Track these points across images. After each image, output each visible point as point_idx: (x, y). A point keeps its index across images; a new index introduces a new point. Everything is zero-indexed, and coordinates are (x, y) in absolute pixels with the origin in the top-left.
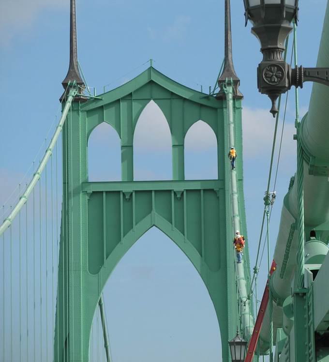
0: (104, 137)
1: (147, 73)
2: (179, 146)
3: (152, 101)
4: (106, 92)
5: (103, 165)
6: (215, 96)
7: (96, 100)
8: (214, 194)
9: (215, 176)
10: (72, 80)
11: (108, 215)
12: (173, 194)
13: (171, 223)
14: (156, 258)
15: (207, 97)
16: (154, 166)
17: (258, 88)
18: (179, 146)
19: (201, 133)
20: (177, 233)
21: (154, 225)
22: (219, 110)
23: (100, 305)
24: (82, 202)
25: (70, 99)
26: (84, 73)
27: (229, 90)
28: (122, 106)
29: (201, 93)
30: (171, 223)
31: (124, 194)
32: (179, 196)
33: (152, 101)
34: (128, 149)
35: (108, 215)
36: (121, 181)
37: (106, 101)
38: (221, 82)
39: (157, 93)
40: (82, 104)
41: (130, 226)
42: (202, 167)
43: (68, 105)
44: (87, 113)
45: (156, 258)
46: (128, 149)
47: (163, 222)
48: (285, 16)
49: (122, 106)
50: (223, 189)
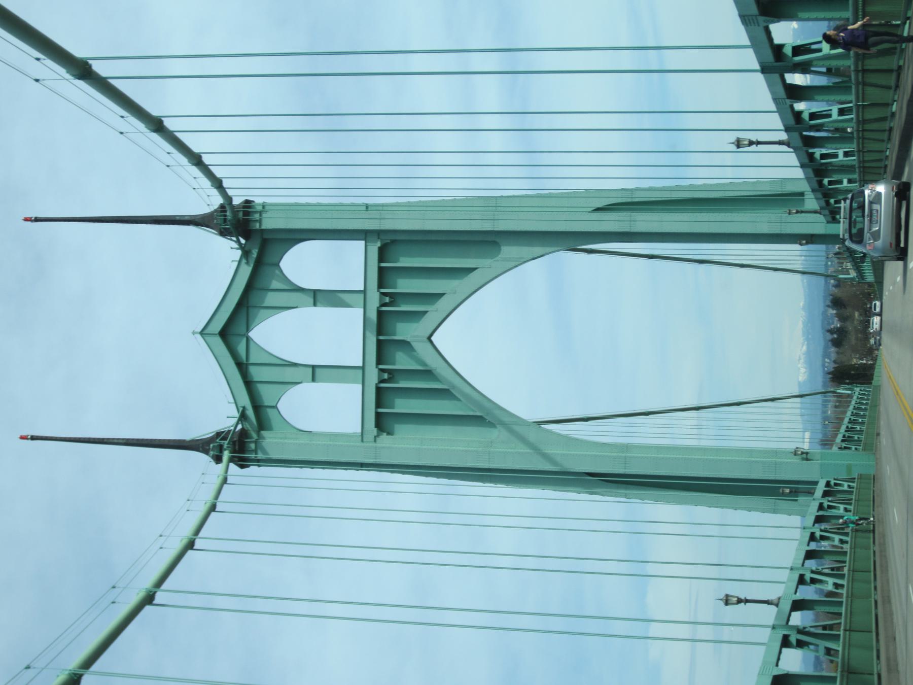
1: (208, 338)
2: (318, 297)
3: (251, 334)
4: (232, 401)
5: (330, 410)
6: (243, 241)
7: (243, 417)
8: (390, 246)
9: (359, 246)
12: (384, 309)
13: (426, 312)
14: (487, 337)
15: (246, 254)
16: (340, 336)
19: (302, 264)
20: (443, 305)
21: (429, 338)
22: (266, 236)
23: (540, 423)
24: (406, 442)
26: (204, 430)
29: (240, 262)
30: (426, 312)
31: (382, 381)
32: (387, 299)
33: (251, 334)
34: (315, 372)
36: (360, 386)
37: (245, 401)
39: (240, 327)
41: (428, 373)
44: (262, 429)
45: (487, 337)
46: (315, 372)
48: (805, 133)
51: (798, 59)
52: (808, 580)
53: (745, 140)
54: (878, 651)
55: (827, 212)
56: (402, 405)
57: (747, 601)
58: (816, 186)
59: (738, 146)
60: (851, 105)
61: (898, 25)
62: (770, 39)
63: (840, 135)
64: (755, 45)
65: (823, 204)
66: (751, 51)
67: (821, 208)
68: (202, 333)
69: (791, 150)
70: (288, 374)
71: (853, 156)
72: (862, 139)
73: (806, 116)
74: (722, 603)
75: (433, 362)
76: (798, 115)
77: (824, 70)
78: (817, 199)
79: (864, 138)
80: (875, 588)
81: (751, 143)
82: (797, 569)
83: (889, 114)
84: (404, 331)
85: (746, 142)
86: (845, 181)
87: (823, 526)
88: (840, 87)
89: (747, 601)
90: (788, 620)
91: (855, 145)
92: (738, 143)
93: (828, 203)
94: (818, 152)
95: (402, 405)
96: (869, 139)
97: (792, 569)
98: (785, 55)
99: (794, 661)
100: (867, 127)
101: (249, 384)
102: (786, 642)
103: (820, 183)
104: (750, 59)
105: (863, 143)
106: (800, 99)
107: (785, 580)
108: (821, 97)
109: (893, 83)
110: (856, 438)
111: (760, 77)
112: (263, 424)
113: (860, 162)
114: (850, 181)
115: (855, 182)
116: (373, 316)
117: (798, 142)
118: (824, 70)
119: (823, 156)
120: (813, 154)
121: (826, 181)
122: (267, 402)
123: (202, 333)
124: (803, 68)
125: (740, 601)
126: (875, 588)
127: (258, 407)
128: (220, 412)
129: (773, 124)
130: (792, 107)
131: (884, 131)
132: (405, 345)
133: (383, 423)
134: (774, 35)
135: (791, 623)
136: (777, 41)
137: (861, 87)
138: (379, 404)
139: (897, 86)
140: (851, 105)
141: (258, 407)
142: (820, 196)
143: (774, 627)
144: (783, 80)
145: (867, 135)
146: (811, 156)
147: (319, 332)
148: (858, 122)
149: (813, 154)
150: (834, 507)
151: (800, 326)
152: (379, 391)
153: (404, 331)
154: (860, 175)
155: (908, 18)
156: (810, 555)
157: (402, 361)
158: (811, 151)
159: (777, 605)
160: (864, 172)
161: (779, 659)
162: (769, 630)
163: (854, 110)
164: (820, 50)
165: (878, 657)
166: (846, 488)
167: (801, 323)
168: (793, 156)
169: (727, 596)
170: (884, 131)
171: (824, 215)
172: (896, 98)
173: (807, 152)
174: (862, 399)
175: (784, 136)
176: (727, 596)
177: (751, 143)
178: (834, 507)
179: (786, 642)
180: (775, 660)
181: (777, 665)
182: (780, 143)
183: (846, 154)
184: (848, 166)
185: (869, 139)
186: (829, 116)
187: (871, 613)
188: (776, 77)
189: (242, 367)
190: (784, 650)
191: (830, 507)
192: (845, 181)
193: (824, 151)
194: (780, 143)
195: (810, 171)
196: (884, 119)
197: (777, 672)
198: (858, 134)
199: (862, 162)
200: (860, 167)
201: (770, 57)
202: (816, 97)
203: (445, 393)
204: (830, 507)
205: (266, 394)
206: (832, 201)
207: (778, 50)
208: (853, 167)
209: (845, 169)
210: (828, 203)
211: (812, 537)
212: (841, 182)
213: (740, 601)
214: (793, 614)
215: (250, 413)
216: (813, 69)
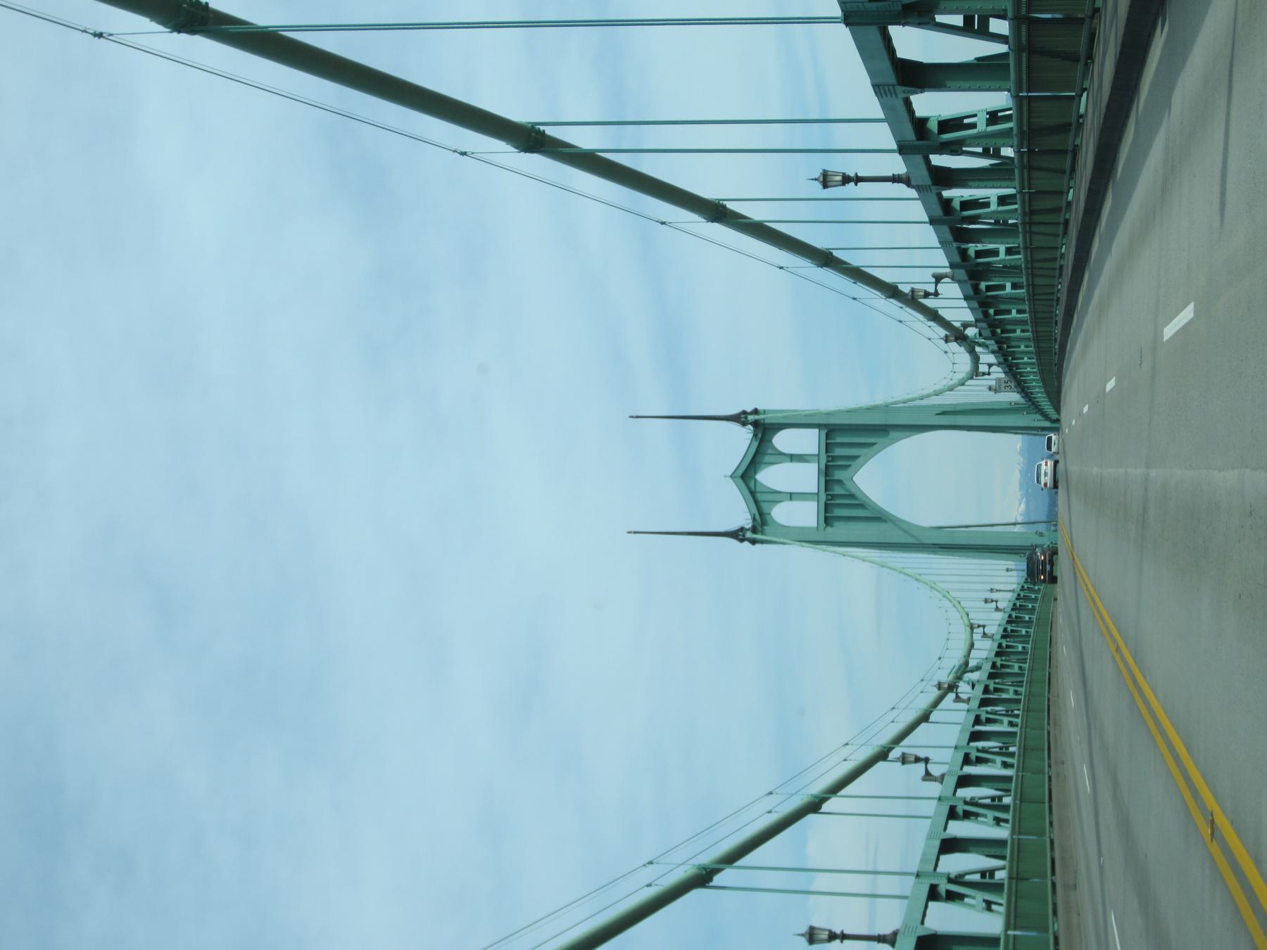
0: (781, 514)
2: (793, 458)
5: (805, 515)
7: (754, 519)
9: (816, 431)
10: (737, 535)
11: (844, 513)
14: (873, 478)
15: (755, 435)
16: (807, 477)
17: (978, 59)
18: (793, 458)
19: (782, 441)
20: (859, 461)
24: (840, 530)
25: (755, 536)
27: (751, 418)
28: (760, 501)
34: (791, 496)
35: (841, 510)
37: (755, 511)
38: (744, 424)
40: (757, 530)
41: (852, 496)
42: (807, 441)
43: (759, 537)
45: (873, 478)
46: (791, 496)
47: (850, 471)
49: (760, 501)
50: (825, 426)
51: (947, 137)
52: (961, 813)
53: (920, 290)
54: (1055, 905)
55: (962, 274)
56: (838, 512)
57: (844, 937)
58: (970, 292)
59: (825, 186)
60: (1010, 125)
61: (1072, 98)
62: (891, 50)
63: (1001, 230)
64: (890, 118)
65: (981, 316)
66: (919, 202)
67: (977, 321)
68: (732, 476)
69: (913, 193)
70: (777, 497)
71: (1019, 253)
72: (1029, 234)
73: (956, 205)
74: (803, 941)
75: (853, 490)
76: (946, 204)
77: (980, 150)
78: (971, 309)
79: (1031, 232)
80: (1051, 824)
81: (846, 180)
82: (947, 799)
83: (1064, 204)
84: (838, 475)
85: (839, 178)
86: (1008, 285)
87: (981, 744)
88: (989, 66)
89: (844, 937)
90: (936, 865)
91: (1020, 239)
92: (826, 180)
93: (986, 314)
94: (972, 248)
95: (838, 512)
96: (1039, 233)
97: (940, 799)
98: (930, 131)
99: (946, 919)
100: (1037, 218)
101: (756, 502)
102: (933, 894)
103: (976, 289)
104: (884, 136)
105: (1030, 178)
106: (950, 186)
107: (948, 760)
108: (957, 84)
109: (1068, 165)
110: (1027, 618)
111: (843, 32)
112: (764, 523)
113: (1026, 261)
114: (1014, 286)
115: (1021, 287)
116: (823, 467)
117: (923, 177)
118: (980, 150)
119: (979, 254)
120: (966, 250)
121: (983, 285)
122: (765, 511)
123: (732, 476)
124: (954, 148)
125: (832, 937)
126: (1051, 824)
127: (761, 514)
128: (741, 516)
129: (875, 144)
130: (939, 195)
131: (1058, 224)
132: (840, 482)
133: (828, 521)
134: (896, 43)
135: (939, 870)
136: (920, 112)
137: (1026, 171)
138: (826, 511)
139: (1073, 170)
140: (1010, 125)
141: (761, 514)
142: (976, 305)
143: (918, 875)
144: (928, 162)
145: (1035, 229)
146: (963, 253)
147: (794, 476)
148: (1024, 214)
149: (949, 201)
150: (1007, 667)
151: (1017, 475)
152: (826, 505)
153: (838, 475)
154: (1027, 280)
155: (1085, 89)
156: (975, 736)
157: (837, 490)
158: (964, 246)
159: (893, 944)
160: (1033, 275)
161: (924, 915)
162: (952, 750)
163: (1014, 118)
164: (973, 126)
165: (1055, 912)
166: (1016, 670)
167: (1017, 473)
168: (918, 205)
169: (812, 929)
170: (1058, 224)
171: (959, 282)
172: (1086, 84)
173: (959, 248)
174: (1026, 598)
175: (897, 165)
176: (812, 929)
177: (846, 180)
178: (1007, 667)
179: (933, 894)
180: (920, 916)
181: (922, 923)
182: (895, 179)
183: (1009, 251)
184: (1012, 267)
185: (1039, 233)
186: (987, 205)
187: (1043, 786)
188: (919, 159)
189: (753, 493)
190: (931, 904)
191: (996, 690)
192: (1014, 312)
193: (980, 247)
194: (895, 179)
195: (945, 229)
196: (1058, 210)
197: (922, 932)
198: (1024, 228)
199: (1030, 261)
200: (1027, 268)
201: (910, 135)
202: (949, 83)
203: (861, 506)
204: (996, 690)
205: (764, 506)
206: (991, 311)
207: (920, 125)
208: (1018, 268)
209: (1008, 270)
210: (986, 314)
211: (977, 721)
212: (1003, 287)
213: (832, 937)
214: (942, 857)
215: (758, 517)
216: (940, 18)
